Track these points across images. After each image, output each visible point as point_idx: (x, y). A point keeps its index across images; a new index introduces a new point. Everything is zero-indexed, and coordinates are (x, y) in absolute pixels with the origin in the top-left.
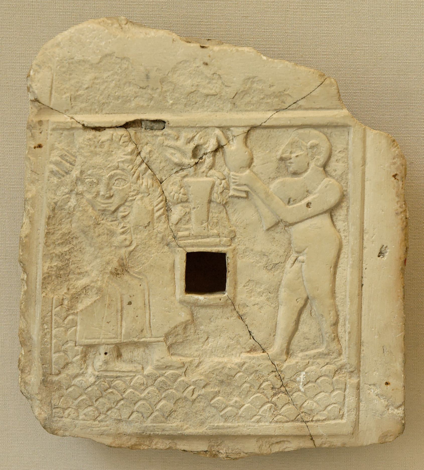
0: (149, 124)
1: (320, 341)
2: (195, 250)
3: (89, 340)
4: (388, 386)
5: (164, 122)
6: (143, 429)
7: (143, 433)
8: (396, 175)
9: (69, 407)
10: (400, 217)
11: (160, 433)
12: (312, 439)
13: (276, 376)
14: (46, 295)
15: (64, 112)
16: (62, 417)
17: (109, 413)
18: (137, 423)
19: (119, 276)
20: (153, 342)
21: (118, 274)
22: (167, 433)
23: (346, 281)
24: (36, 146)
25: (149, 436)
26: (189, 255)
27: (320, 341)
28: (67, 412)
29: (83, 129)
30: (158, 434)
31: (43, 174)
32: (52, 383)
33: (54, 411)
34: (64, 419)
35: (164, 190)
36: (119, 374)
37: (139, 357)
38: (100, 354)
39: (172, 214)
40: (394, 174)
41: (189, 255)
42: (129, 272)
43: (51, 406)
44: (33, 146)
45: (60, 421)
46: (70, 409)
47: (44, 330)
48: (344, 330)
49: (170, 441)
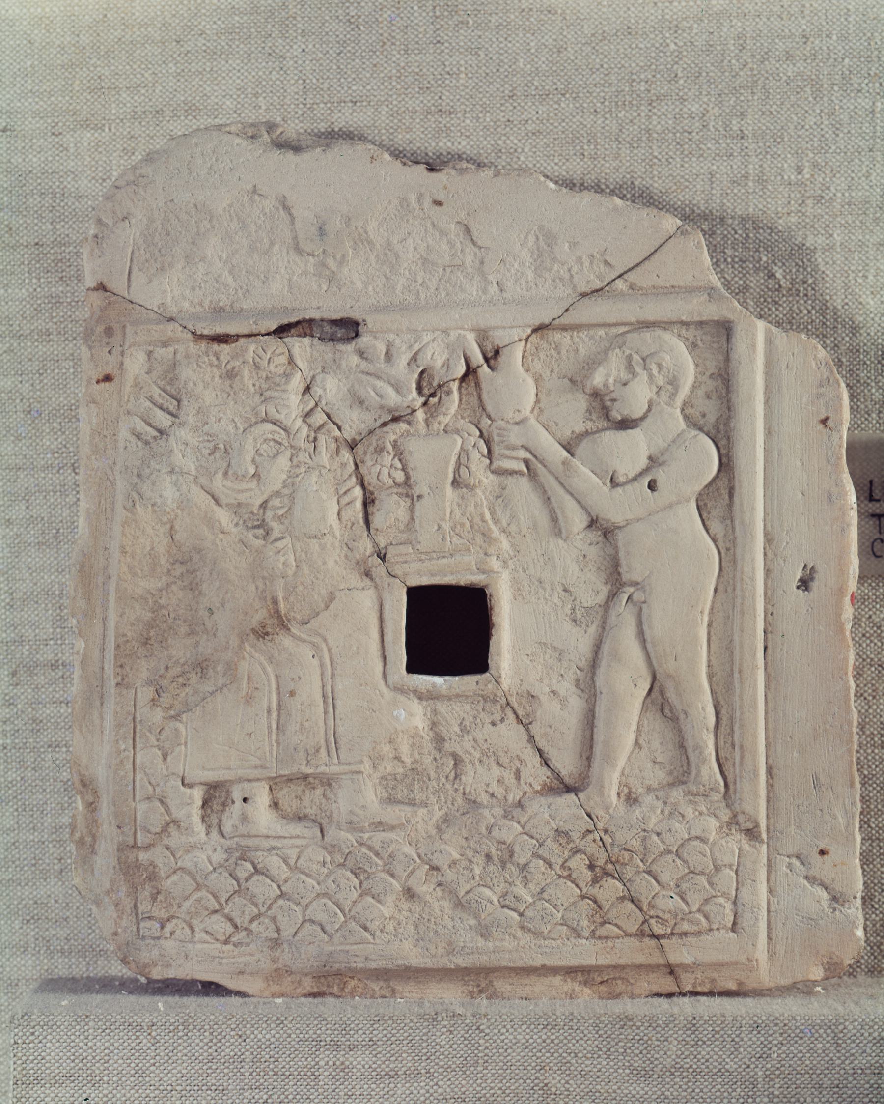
0: (327, 328)
1: (682, 766)
2: (425, 581)
3: (211, 773)
4: (826, 857)
5: (357, 324)
6: (324, 958)
7: (325, 966)
8: (827, 418)
9: (173, 917)
10: (399, 988)
11: (360, 966)
12: (672, 973)
13: (594, 841)
14: (123, 679)
15: (391, 686)
16: (158, 938)
17: (254, 925)
18: (312, 946)
19: (270, 637)
20: (342, 774)
21: (267, 634)
22: (373, 965)
23: (731, 641)
24: (101, 378)
25: (338, 974)
26: (417, 595)
27: (682, 766)
28: (169, 928)
29: (193, 341)
30: (356, 968)
31: (115, 435)
32: (138, 865)
33: (142, 925)
34: (162, 942)
35: (358, 462)
36: (274, 843)
37: (314, 807)
38: (233, 802)
39: (375, 511)
40: (823, 417)
41: (417, 595)
42: (289, 629)
43: (137, 915)
44: (95, 378)
45: (154, 946)
46: (174, 921)
47: (119, 752)
48: (730, 742)
49: (381, 983)
